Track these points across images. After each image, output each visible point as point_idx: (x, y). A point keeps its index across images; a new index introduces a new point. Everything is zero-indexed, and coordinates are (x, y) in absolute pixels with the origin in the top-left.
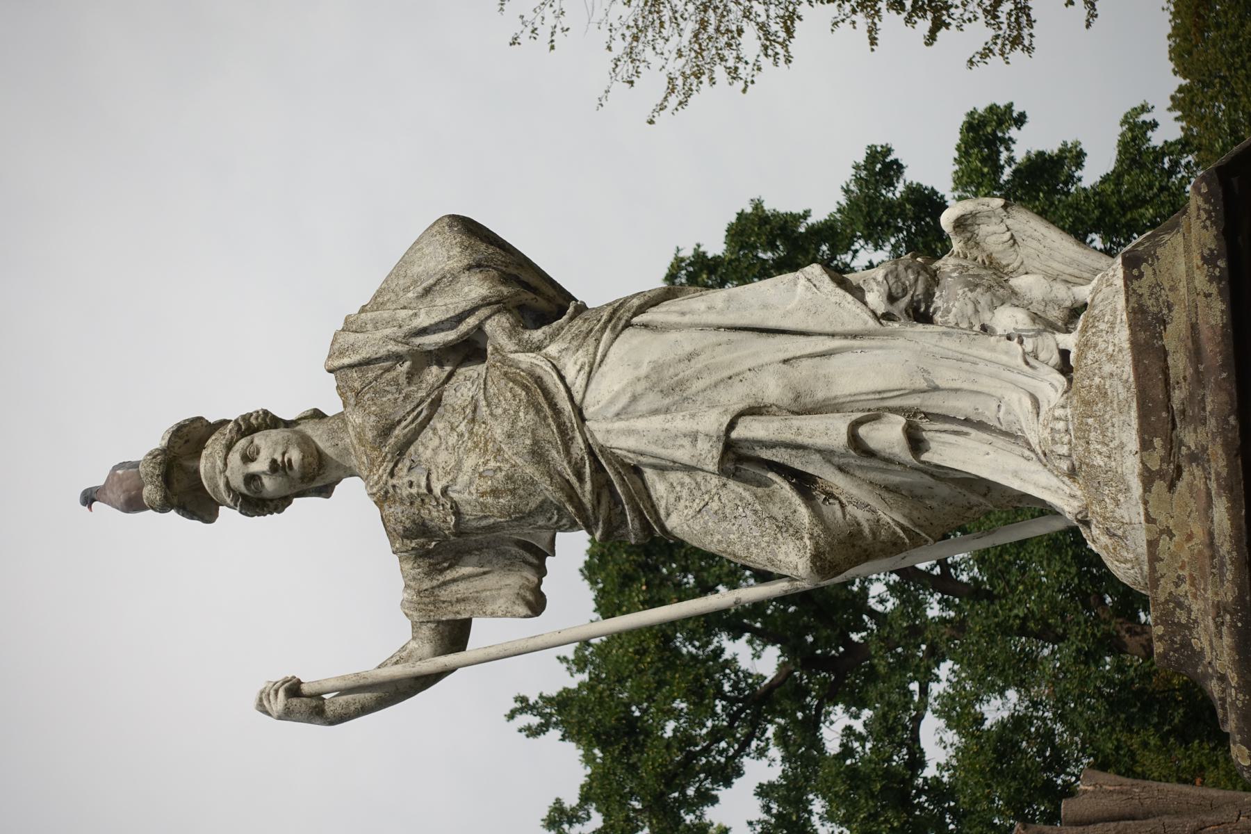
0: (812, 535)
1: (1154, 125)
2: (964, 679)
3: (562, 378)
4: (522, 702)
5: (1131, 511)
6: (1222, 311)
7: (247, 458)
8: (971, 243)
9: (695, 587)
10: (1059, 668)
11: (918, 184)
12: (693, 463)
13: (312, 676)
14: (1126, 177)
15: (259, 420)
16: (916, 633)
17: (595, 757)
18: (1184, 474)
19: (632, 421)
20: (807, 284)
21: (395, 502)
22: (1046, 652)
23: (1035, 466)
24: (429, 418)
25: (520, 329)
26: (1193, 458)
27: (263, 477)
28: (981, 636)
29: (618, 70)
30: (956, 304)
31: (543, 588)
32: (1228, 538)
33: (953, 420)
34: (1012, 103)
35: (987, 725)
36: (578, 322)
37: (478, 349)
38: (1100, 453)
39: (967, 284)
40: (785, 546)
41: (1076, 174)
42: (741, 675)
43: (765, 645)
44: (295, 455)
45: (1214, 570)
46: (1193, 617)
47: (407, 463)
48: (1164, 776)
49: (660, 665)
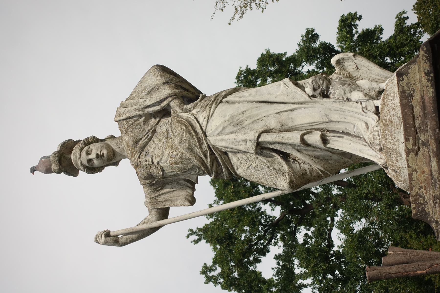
0: (289, 174)
1: (407, 18)
2: (346, 215)
3: (198, 122)
4: (191, 231)
5: (402, 163)
6: (433, 92)
7: (88, 154)
8: (342, 69)
9: (250, 186)
10: (380, 211)
11: (324, 42)
12: (246, 151)
13: (113, 230)
14: (398, 37)
15: (92, 140)
16: (328, 200)
17: (217, 248)
18: (421, 150)
19: (223, 136)
20: (284, 85)
21: (141, 167)
22: (375, 205)
23: (367, 148)
24: (152, 137)
25: (183, 105)
26: (424, 144)
27: (94, 160)
28: (352, 200)
29: (217, 6)
30: (338, 91)
31: (194, 195)
32: (437, 173)
33: (338, 132)
34: (357, 12)
35: (355, 232)
36: (203, 101)
37: (168, 112)
38: (391, 143)
39: (341, 84)
40: (280, 179)
41: (380, 36)
42: (268, 217)
43: (276, 206)
44: (105, 152)
45: (432, 184)
46: (425, 201)
47: (144, 153)
48: (418, 248)
49: (239, 214)
